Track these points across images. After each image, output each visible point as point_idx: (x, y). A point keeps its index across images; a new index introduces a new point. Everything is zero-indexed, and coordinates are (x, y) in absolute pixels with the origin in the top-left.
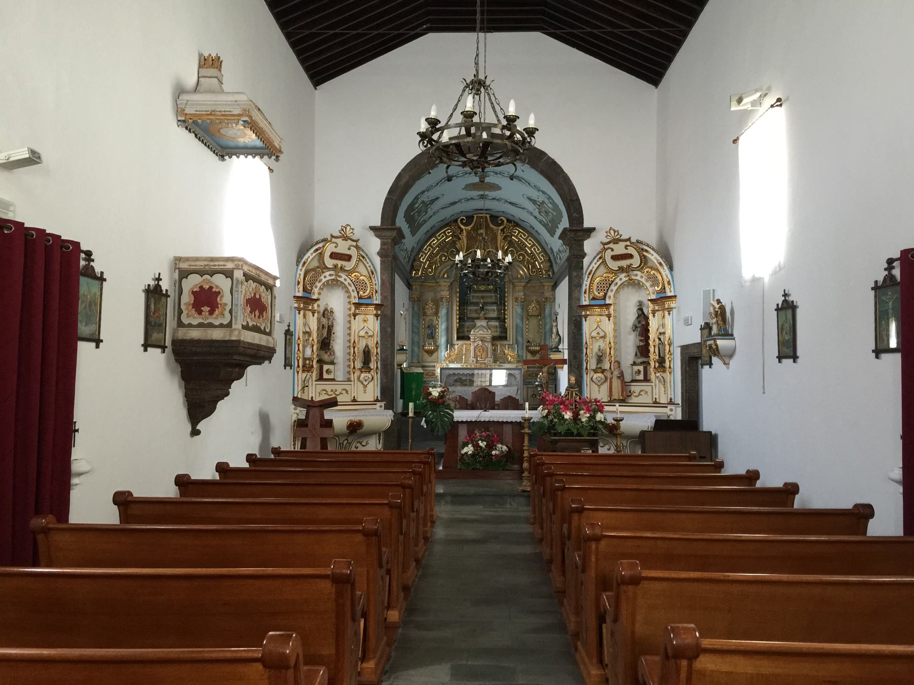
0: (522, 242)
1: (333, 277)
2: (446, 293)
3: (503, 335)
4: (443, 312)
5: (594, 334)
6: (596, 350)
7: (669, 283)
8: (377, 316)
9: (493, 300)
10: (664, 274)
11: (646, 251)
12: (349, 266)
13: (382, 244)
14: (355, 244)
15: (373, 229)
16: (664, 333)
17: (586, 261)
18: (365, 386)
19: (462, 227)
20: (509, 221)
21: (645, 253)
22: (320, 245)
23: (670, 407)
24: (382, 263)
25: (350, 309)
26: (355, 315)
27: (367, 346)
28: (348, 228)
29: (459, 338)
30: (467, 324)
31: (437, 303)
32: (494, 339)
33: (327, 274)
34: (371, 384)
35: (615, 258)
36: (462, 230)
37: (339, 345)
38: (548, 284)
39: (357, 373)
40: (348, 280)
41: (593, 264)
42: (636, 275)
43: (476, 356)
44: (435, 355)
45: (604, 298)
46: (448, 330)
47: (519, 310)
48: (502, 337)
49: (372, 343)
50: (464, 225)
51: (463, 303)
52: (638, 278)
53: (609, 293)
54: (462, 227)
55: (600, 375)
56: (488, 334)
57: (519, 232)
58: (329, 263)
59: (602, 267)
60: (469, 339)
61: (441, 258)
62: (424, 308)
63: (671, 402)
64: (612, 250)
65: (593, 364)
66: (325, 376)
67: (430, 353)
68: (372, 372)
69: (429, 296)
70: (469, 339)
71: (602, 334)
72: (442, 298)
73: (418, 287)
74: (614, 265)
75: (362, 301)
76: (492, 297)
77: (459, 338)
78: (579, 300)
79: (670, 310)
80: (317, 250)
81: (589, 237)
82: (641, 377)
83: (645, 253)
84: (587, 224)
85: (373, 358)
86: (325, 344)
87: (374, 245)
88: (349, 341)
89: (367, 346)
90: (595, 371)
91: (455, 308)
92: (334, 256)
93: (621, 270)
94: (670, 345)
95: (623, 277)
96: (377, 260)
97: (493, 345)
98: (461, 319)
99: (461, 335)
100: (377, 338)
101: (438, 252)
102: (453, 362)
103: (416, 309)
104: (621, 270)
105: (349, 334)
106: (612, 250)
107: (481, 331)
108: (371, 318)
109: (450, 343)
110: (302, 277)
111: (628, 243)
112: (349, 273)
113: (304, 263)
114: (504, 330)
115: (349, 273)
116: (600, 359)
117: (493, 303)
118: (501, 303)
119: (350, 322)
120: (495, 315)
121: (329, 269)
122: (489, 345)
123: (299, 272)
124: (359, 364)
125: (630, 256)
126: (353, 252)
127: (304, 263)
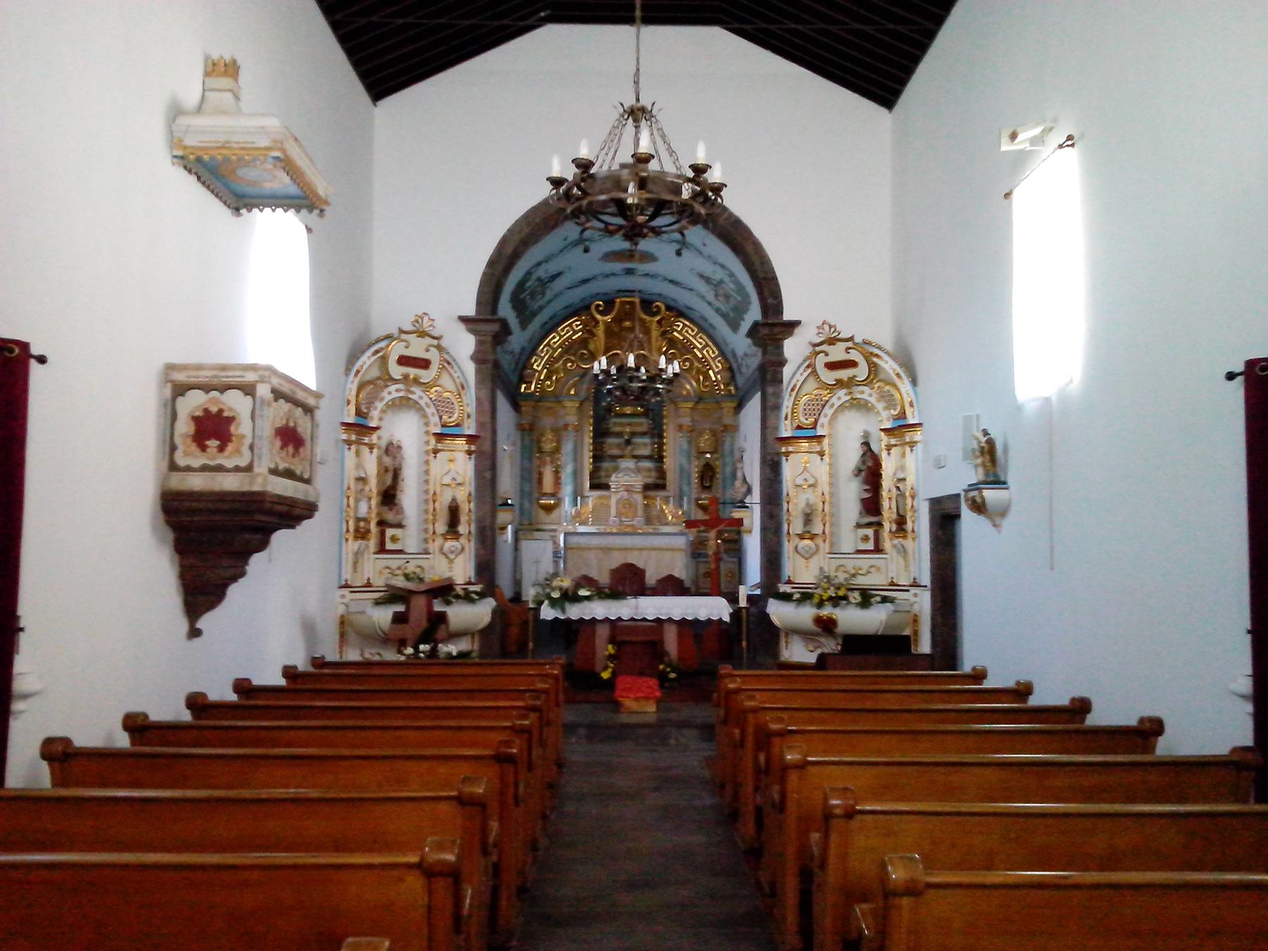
0: (689, 340)
1: (401, 394)
2: (572, 419)
3: (660, 482)
4: (568, 447)
5: (799, 481)
6: (802, 505)
7: (911, 405)
8: (469, 453)
9: (644, 429)
10: (903, 391)
11: (877, 356)
12: (425, 375)
13: (480, 343)
14: (435, 342)
15: (464, 320)
16: (904, 479)
17: (787, 371)
18: (451, 561)
19: (598, 317)
20: (669, 308)
21: (875, 359)
22: (382, 344)
23: (913, 590)
24: (478, 372)
25: (427, 443)
26: (436, 452)
27: (454, 500)
28: (426, 319)
29: (593, 487)
30: (606, 465)
31: (559, 432)
32: (647, 487)
33: (393, 388)
34: (461, 557)
35: (832, 366)
36: (597, 322)
37: (409, 498)
38: (729, 405)
39: (439, 541)
40: (426, 399)
41: (798, 375)
42: (863, 392)
43: (619, 515)
44: (555, 514)
45: (814, 428)
46: (576, 474)
47: (685, 446)
48: (657, 485)
49: (462, 495)
50: (601, 313)
51: (601, 434)
52: (865, 396)
53: (822, 420)
54: (598, 317)
55: (807, 542)
56: (637, 481)
57: (685, 325)
58: (396, 371)
59: (811, 380)
60: (607, 487)
61: (565, 364)
62: (539, 442)
63: (915, 584)
64: (827, 355)
65: (797, 527)
66: (389, 546)
67: (549, 509)
68: (462, 540)
69: (547, 422)
70: (607, 487)
71: (811, 481)
72: (566, 426)
73: (530, 409)
74: (829, 377)
75: (447, 431)
76: (643, 424)
77: (593, 487)
78: (776, 429)
79: (912, 444)
80: (377, 352)
81: (791, 334)
82: (870, 546)
83: (875, 359)
84: (788, 316)
85: (464, 518)
86: (389, 497)
87: (464, 345)
88: (427, 492)
89: (454, 500)
90: (801, 537)
91: (588, 440)
92: (404, 361)
93: (840, 383)
94: (913, 497)
95: (842, 395)
96: (470, 369)
97: (645, 497)
98: (598, 458)
99: (596, 481)
100: (470, 487)
101: (561, 355)
102: (583, 523)
103: (527, 442)
104: (840, 383)
105: (427, 482)
106: (827, 355)
107: (627, 477)
108: (461, 457)
109: (577, 493)
110: (354, 393)
111: (850, 344)
112: (426, 386)
113: (358, 372)
114: (662, 474)
115: (426, 386)
116: (808, 518)
117: (643, 434)
118: (657, 433)
119: (427, 462)
120: (646, 451)
121: (396, 381)
122: (639, 498)
123: (349, 386)
124: (441, 527)
125: (852, 364)
126: (433, 356)
127: (358, 372)
